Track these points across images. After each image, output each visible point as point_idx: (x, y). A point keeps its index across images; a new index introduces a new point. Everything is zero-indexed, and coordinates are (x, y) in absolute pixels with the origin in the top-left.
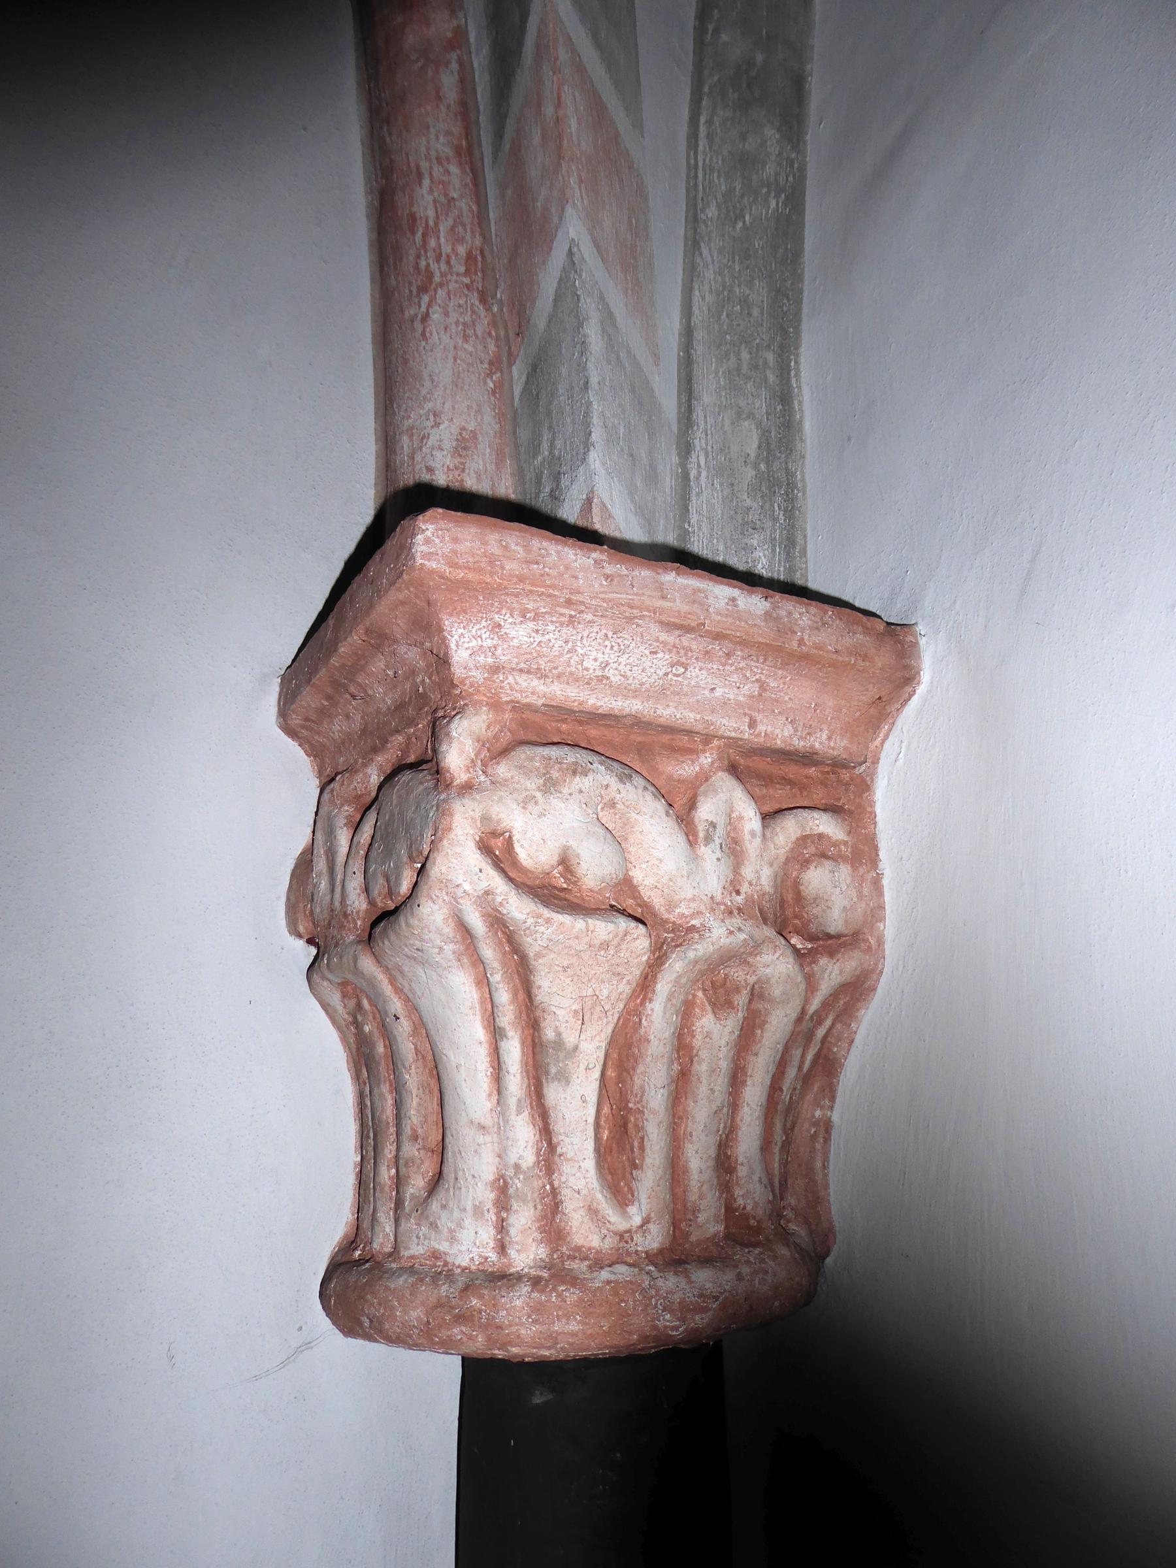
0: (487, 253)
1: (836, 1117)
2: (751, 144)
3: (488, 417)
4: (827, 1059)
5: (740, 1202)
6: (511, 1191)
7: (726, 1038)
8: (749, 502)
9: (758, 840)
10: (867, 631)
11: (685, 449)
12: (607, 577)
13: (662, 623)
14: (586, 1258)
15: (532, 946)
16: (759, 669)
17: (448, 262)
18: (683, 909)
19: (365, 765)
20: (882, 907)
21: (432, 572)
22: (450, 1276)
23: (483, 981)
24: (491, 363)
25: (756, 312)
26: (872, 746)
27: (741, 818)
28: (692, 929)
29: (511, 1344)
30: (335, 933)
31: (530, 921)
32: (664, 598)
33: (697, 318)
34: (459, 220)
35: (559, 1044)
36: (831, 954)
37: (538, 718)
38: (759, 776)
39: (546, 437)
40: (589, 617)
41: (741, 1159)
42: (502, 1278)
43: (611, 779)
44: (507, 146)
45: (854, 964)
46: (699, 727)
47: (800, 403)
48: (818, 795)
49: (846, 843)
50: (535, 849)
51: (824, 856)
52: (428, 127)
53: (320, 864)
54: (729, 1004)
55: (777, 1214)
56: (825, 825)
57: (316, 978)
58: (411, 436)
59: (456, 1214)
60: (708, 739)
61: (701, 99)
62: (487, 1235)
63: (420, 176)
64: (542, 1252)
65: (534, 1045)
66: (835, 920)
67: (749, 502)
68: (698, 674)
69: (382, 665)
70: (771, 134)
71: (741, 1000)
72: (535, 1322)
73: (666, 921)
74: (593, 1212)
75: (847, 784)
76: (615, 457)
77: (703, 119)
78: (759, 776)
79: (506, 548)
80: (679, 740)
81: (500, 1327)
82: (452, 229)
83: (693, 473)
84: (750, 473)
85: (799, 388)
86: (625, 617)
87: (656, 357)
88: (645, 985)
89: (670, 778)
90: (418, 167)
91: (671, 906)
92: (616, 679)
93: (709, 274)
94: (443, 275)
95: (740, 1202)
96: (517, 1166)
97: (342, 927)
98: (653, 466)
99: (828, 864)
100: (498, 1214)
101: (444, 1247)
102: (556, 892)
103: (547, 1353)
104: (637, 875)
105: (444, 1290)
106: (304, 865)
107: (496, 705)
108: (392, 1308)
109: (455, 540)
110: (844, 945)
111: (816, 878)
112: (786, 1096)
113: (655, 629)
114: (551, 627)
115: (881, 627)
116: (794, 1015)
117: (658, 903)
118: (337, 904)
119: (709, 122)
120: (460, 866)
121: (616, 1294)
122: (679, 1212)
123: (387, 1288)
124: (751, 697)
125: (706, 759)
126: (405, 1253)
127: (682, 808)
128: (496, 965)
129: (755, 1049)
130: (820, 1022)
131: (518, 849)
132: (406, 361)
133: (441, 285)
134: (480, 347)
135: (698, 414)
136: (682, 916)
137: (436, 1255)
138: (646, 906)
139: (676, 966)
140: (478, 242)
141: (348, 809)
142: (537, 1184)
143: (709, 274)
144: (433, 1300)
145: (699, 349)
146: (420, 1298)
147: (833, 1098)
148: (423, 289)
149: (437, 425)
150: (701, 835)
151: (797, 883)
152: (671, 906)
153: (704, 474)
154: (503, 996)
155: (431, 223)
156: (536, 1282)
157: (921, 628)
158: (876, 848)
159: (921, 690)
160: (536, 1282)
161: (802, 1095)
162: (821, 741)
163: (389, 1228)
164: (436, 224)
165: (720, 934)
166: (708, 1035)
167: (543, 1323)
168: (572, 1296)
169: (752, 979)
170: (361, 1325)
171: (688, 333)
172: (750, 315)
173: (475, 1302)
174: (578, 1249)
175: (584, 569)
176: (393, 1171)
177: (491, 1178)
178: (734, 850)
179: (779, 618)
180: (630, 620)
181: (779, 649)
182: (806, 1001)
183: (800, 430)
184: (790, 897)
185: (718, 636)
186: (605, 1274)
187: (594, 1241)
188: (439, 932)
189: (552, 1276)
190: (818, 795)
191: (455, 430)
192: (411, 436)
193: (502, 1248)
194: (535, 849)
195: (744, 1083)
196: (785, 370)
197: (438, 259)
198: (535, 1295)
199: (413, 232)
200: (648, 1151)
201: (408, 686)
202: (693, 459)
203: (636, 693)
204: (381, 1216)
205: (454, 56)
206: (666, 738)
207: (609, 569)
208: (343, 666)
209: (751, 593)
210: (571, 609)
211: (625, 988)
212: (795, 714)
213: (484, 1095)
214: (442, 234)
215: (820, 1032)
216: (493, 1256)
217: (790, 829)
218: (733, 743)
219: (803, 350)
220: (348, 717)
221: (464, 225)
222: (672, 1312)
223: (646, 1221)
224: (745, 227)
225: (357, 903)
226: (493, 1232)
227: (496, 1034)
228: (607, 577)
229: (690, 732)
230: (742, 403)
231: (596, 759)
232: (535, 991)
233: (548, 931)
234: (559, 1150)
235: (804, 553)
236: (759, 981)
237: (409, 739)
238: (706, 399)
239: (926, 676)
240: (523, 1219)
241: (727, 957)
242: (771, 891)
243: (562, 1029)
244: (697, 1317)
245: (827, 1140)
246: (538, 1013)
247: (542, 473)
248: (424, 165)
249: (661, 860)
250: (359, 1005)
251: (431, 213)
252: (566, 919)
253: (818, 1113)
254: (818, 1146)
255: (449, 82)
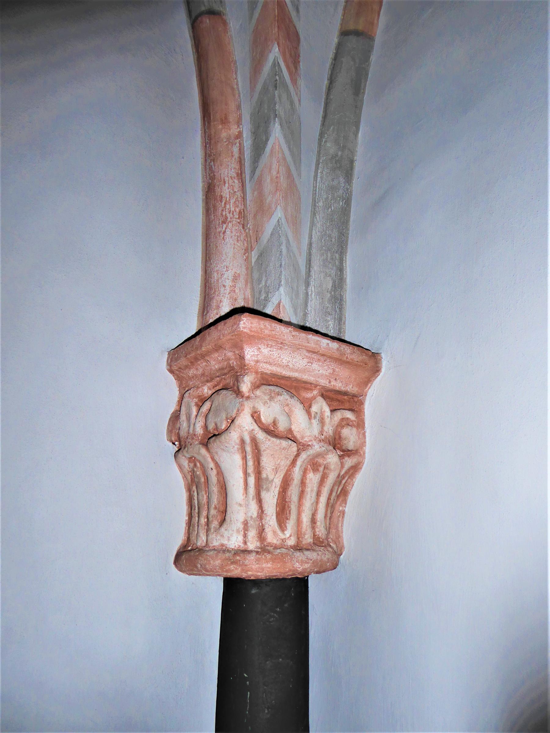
0: (245, 211)
1: (347, 510)
2: (335, 183)
3: (244, 269)
4: (345, 491)
5: (318, 533)
6: (249, 525)
7: (316, 481)
8: (328, 305)
9: (329, 419)
10: (367, 355)
11: (307, 284)
12: (293, 336)
13: (307, 350)
14: (272, 546)
15: (262, 447)
16: (333, 365)
17: (233, 214)
18: (306, 439)
19: (202, 386)
20: (365, 442)
21: (245, 332)
22: (229, 551)
23: (244, 458)
24: (245, 250)
25: (333, 240)
26: (365, 391)
27: (324, 411)
28: (309, 445)
29: (249, 571)
30: (190, 440)
31: (264, 439)
32: (308, 343)
33: (314, 239)
34: (237, 200)
35: (267, 479)
36: (349, 456)
37: (267, 377)
38: (329, 398)
39: (264, 279)
40: (286, 347)
41: (318, 520)
42: (246, 552)
43: (287, 397)
44: (256, 177)
45: (356, 460)
46: (314, 382)
47: (346, 272)
48: (347, 405)
49: (355, 421)
50: (266, 419)
51: (348, 425)
52: (228, 166)
53: (183, 417)
54: (318, 470)
55: (327, 538)
56: (349, 415)
57: (180, 455)
58: (218, 273)
59: (231, 532)
60: (316, 386)
61: (319, 164)
62: (241, 538)
63: (225, 183)
64: (258, 544)
65: (259, 479)
66: (351, 446)
67: (328, 305)
68: (315, 366)
69: (216, 355)
70: (342, 180)
71: (321, 469)
72: (257, 564)
73: (301, 443)
74: (274, 532)
75: (356, 402)
76: (287, 289)
77: (319, 171)
78: (329, 398)
79: (265, 326)
80: (307, 386)
81: (246, 565)
82: (235, 202)
83: (310, 293)
84: (329, 295)
85: (346, 267)
86: (296, 348)
87: (300, 253)
88: (294, 463)
89: (304, 397)
90: (224, 180)
91: (303, 438)
92: (291, 366)
93: (319, 225)
94: (231, 218)
95: (318, 533)
96: (251, 517)
97: (193, 439)
98: (298, 291)
99: (350, 427)
100: (244, 532)
101: (225, 542)
102: (271, 431)
103: (259, 574)
104: (293, 427)
105: (227, 555)
106: (175, 417)
107: (257, 373)
108: (209, 561)
109: (252, 323)
110: (353, 454)
111: (346, 432)
112: (332, 501)
113: (305, 352)
114: (275, 350)
115: (370, 354)
116: (337, 475)
117: (298, 436)
118: (191, 431)
119: (322, 173)
120: (245, 422)
121: (282, 556)
122: (299, 535)
123: (206, 555)
124: (330, 373)
125: (315, 392)
126: (211, 545)
127: (307, 406)
128: (250, 453)
129: (324, 485)
130: (344, 478)
131: (262, 417)
132: (217, 247)
133: (230, 222)
134: (242, 244)
135: (312, 273)
136: (306, 441)
137: (222, 545)
138: (295, 437)
139: (304, 456)
140: (243, 207)
141: (196, 400)
142: (257, 523)
143: (319, 225)
144: (224, 557)
145: (314, 251)
146: (219, 557)
147: (346, 504)
148: (224, 222)
149: (227, 271)
150: (313, 416)
151: (340, 433)
152: (303, 438)
153: (313, 294)
154: (250, 463)
155: (228, 200)
156: (257, 552)
157: (383, 355)
158: (364, 423)
159: (382, 374)
160: (257, 552)
161: (336, 503)
162: (351, 388)
163: (204, 538)
164: (229, 200)
165: (317, 448)
166: (311, 480)
167: (260, 564)
168: (269, 556)
169: (325, 463)
170: (197, 567)
171: (310, 244)
172: (331, 241)
173: (238, 558)
174: (269, 543)
175: (287, 333)
176: (206, 520)
177: (243, 520)
178: (322, 422)
179: (341, 350)
180: (298, 349)
181: (340, 360)
182: (340, 471)
183: (345, 282)
184: (337, 437)
185: (323, 355)
186: (278, 551)
187: (275, 541)
188: (235, 442)
189: (263, 551)
190: (347, 405)
191: (233, 273)
192: (218, 273)
193: (245, 543)
194: (266, 419)
195: (320, 496)
196: (341, 261)
197: (230, 213)
198: (258, 556)
199: (221, 202)
200: (292, 514)
201: (226, 363)
202: (310, 288)
203: (297, 371)
204: (201, 535)
205: (238, 141)
206: (303, 385)
207: (294, 333)
208: (201, 354)
209: (333, 342)
210: (281, 344)
211: (288, 463)
212: (344, 381)
213: (241, 495)
214: (231, 204)
215: (344, 482)
216: (242, 545)
217: (339, 415)
218: (323, 387)
219: (348, 254)
220: (197, 369)
221: (238, 201)
222: (299, 563)
223: (291, 536)
224: (332, 211)
225: (199, 430)
226: (242, 537)
227: (246, 474)
228: (293, 336)
229: (311, 384)
230: (328, 271)
231: (284, 390)
232: (261, 462)
233: (268, 443)
234: (265, 512)
235: (344, 323)
236: (327, 463)
237: (222, 379)
238: (315, 268)
239: (383, 370)
240: (252, 534)
241: (319, 455)
242: (332, 435)
243: (269, 474)
244: (306, 565)
245: (343, 517)
246: (261, 469)
247: (261, 291)
248: (226, 179)
249: (301, 424)
250: (195, 465)
251: (228, 196)
252: (274, 439)
253: (341, 508)
254: (340, 519)
255: (236, 150)
